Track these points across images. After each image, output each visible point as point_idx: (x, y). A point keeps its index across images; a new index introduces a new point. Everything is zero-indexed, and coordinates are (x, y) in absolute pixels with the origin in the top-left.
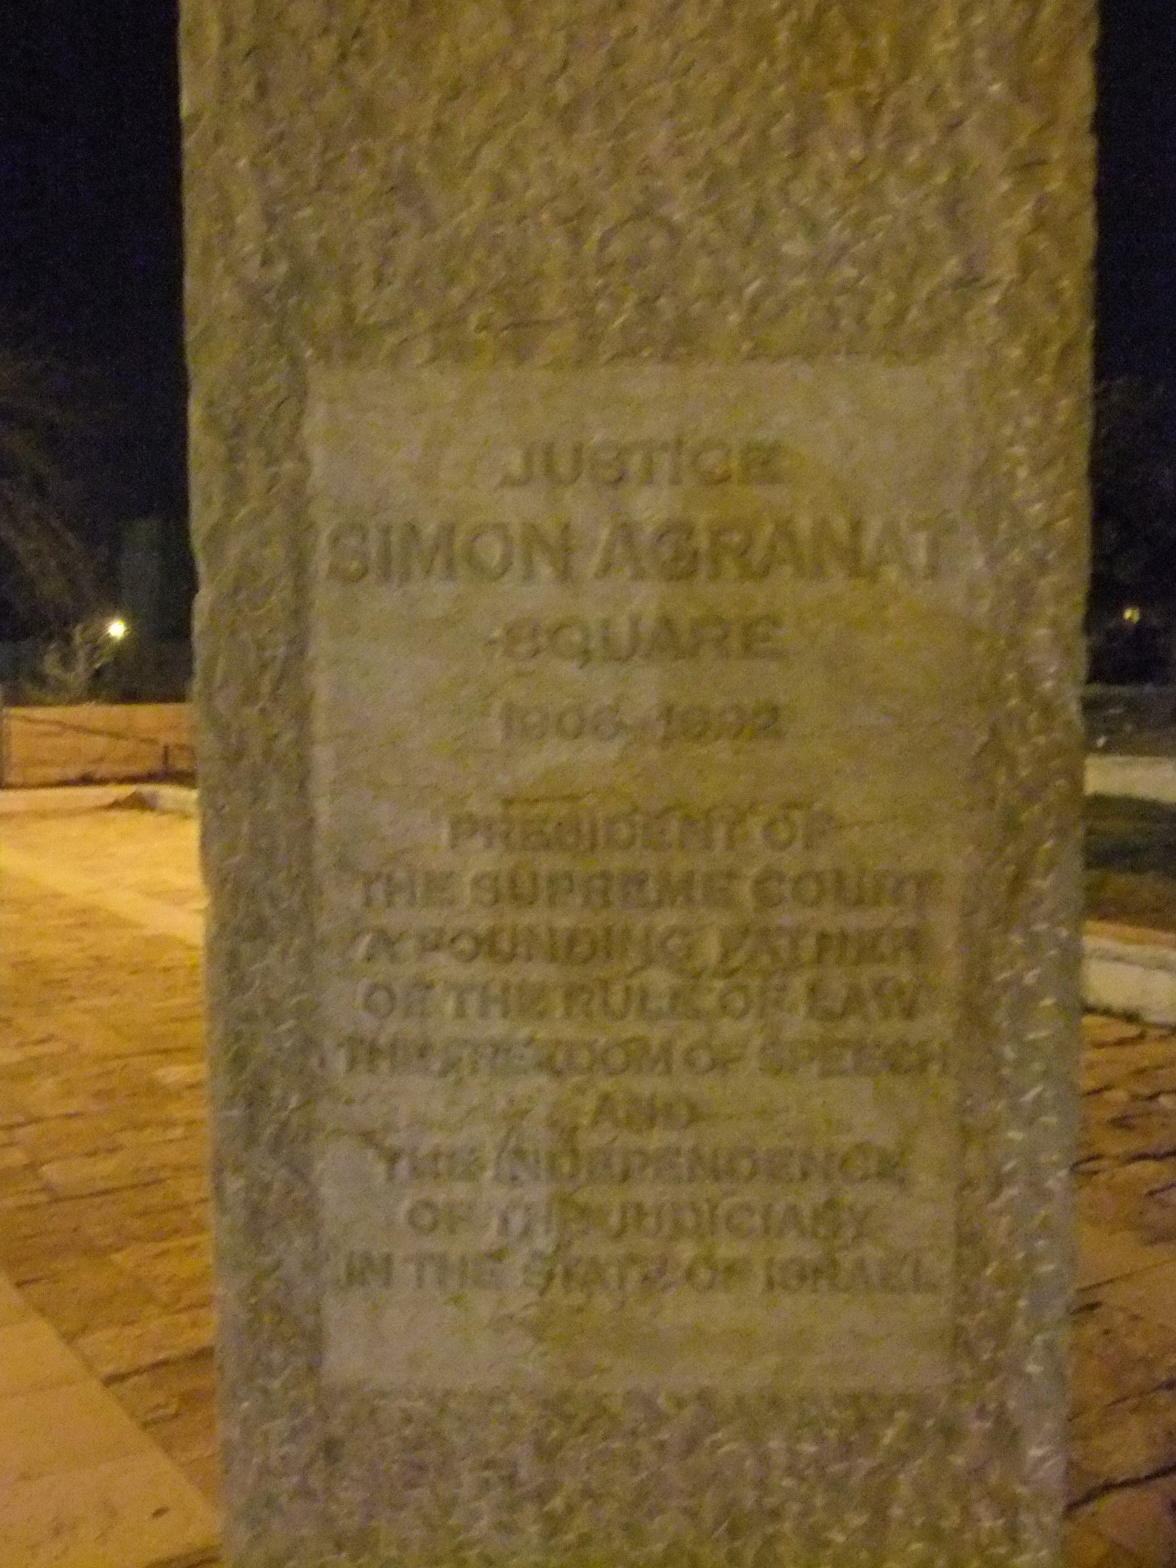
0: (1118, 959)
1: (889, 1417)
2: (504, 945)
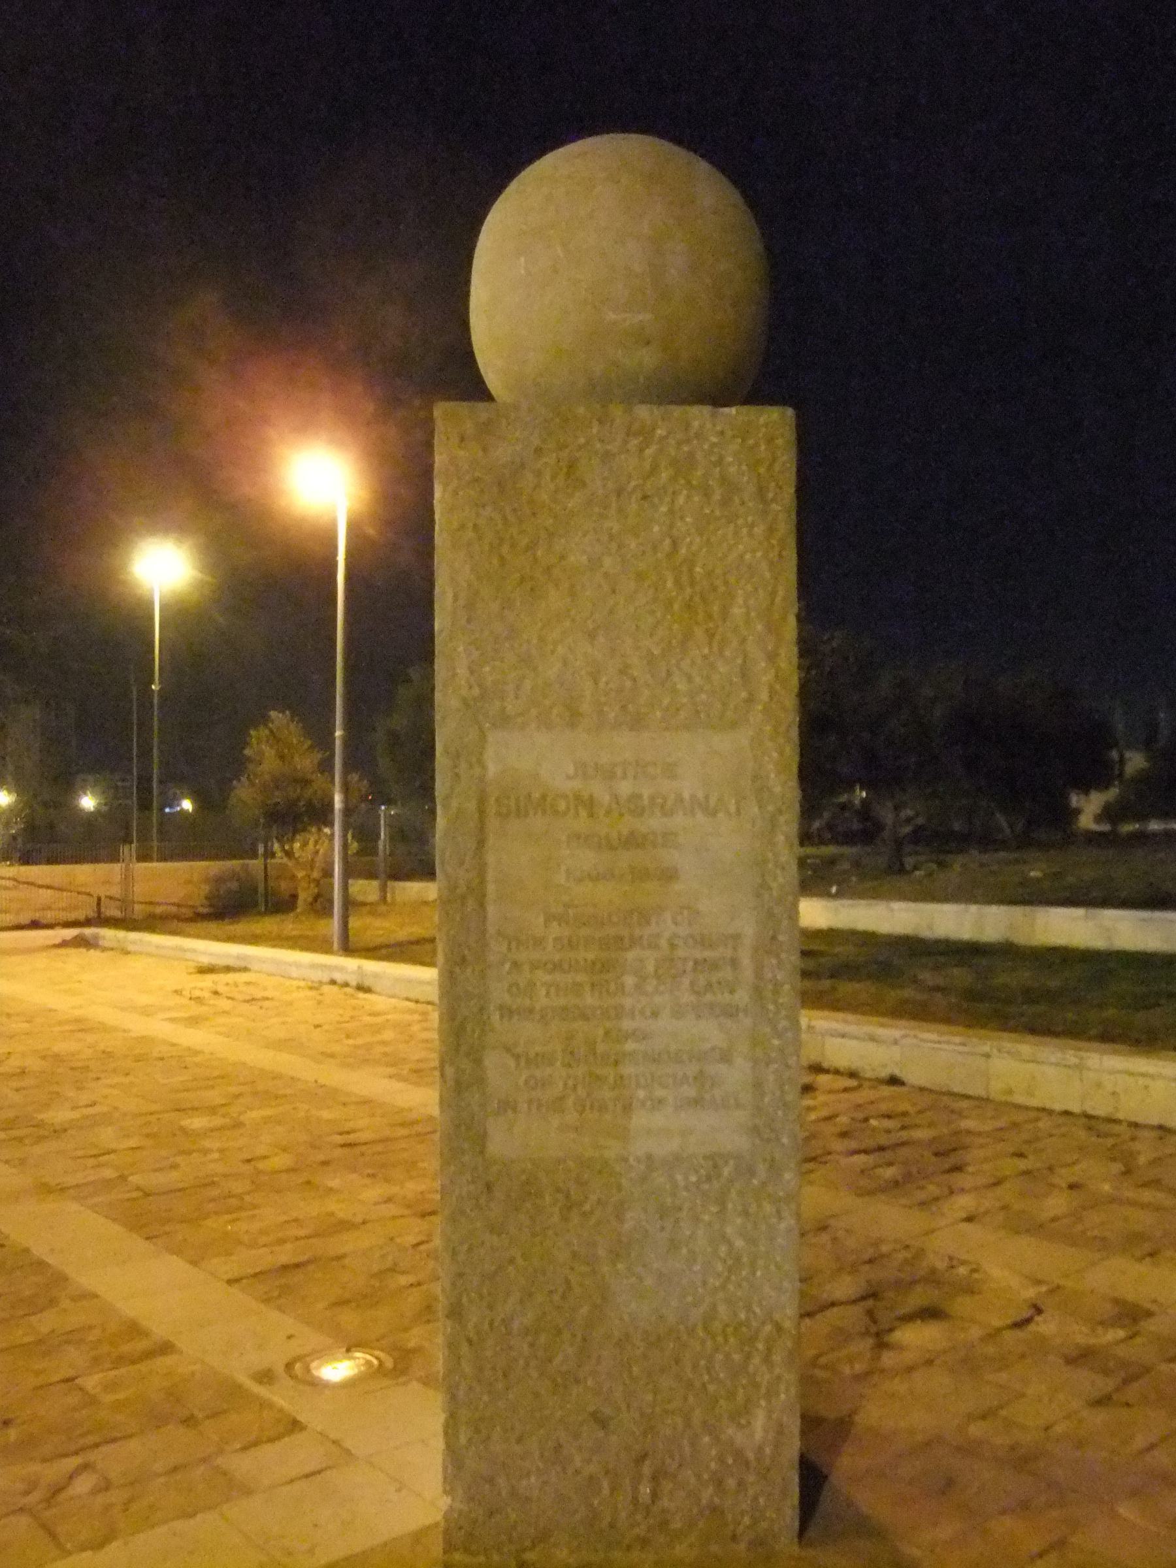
0: (843, 1036)
1: (726, 1162)
2: (566, 967)
